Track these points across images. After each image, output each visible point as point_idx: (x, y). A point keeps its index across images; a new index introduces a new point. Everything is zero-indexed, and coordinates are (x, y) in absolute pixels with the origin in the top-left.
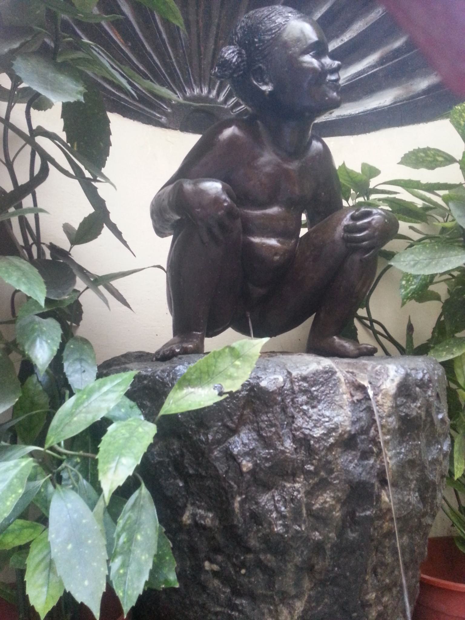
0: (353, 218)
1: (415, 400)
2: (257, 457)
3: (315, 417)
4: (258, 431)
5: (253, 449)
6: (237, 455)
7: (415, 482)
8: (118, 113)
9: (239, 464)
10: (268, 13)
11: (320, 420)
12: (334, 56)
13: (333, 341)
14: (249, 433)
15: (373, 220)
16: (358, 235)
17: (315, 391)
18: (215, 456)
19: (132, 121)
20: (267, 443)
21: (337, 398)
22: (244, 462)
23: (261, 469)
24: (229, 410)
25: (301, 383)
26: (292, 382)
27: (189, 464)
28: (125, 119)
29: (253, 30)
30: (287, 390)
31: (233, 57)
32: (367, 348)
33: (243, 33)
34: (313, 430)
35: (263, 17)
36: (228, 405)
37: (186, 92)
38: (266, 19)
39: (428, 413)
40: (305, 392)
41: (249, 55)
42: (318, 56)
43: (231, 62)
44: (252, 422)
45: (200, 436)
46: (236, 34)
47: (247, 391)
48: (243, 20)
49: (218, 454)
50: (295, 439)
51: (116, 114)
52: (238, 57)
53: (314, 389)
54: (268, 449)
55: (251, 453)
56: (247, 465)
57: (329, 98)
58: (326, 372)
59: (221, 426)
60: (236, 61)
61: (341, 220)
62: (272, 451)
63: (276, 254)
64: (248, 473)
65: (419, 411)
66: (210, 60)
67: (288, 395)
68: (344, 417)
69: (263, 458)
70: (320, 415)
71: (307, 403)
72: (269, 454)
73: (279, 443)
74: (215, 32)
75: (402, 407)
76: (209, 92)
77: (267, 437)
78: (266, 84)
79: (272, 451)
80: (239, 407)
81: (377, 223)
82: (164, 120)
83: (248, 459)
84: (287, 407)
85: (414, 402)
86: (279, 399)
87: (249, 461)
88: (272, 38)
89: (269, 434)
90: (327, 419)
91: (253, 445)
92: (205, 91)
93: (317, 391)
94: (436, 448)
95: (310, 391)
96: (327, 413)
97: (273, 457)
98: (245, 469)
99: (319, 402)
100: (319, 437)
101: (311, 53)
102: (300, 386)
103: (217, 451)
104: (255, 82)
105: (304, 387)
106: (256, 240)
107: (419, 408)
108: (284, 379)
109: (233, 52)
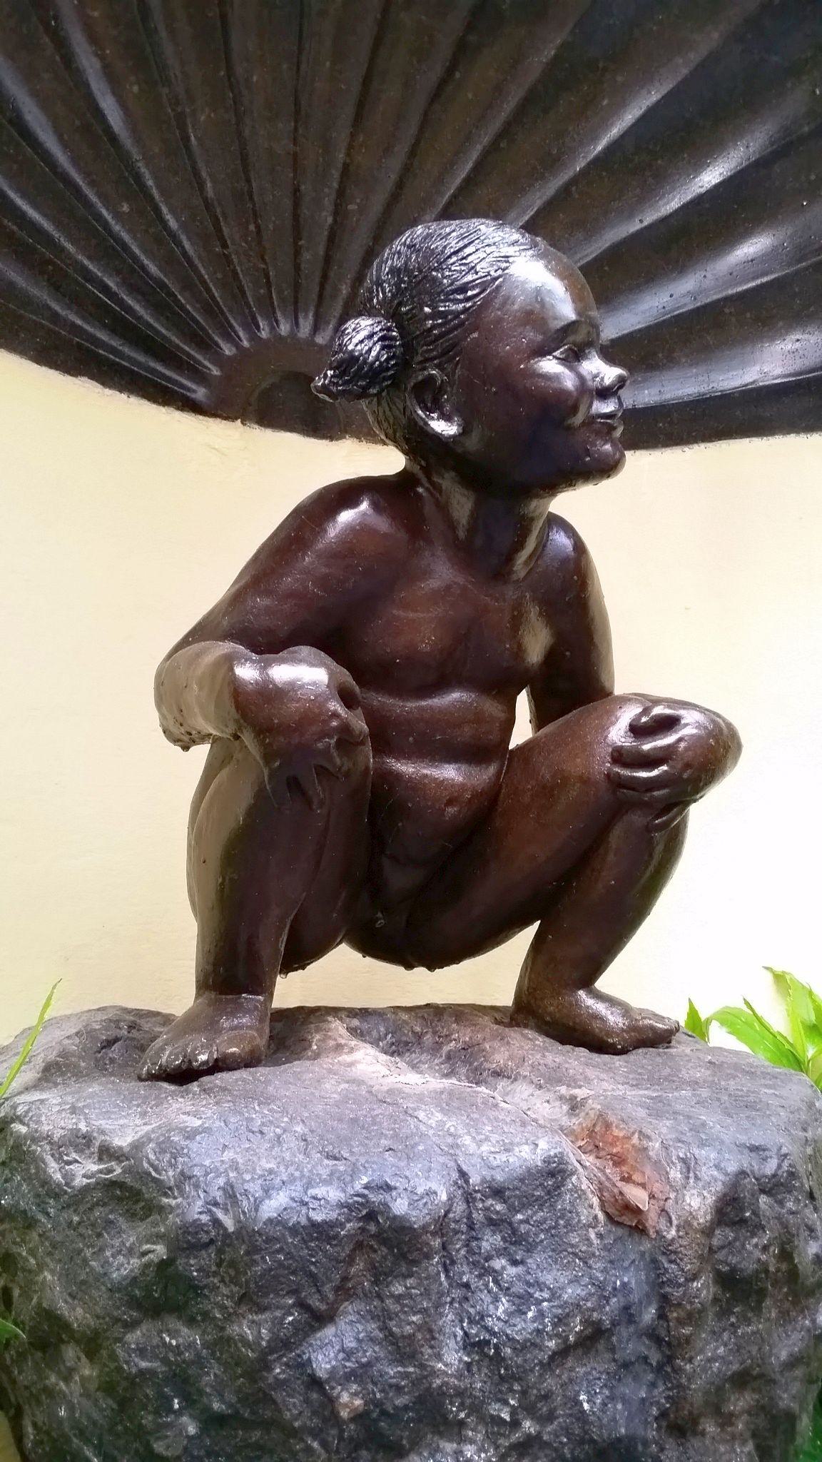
0: (637, 730)
1: (758, 1228)
2: (375, 1384)
3: (519, 1288)
4: (383, 1318)
5: (369, 1365)
6: (328, 1381)
7: (745, 1417)
8: (92, 377)
9: (331, 1401)
10: (461, 244)
11: (531, 1296)
12: (611, 353)
13: (578, 1004)
14: (359, 1322)
15: (680, 740)
16: (643, 774)
17: (521, 1222)
18: (275, 1377)
19: (124, 396)
20: (403, 1349)
21: (574, 1238)
22: (345, 1397)
23: (384, 1413)
24: (312, 1268)
25: (490, 1202)
26: (469, 1198)
27: (212, 1387)
28: (108, 391)
29: (420, 282)
30: (456, 1222)
31: (370, 350)
32: (652, 1028)
33: (397, 285)
34: (512, 1321)
35: (448, 252)
36: (312, 1256)
37: (258, 328)
38: (454, 259)
39: (786, 1255)
40: (494, 1223)
41: (408, 347)
42: (574, 357)
43: (365, 361)
44: (367, 1296)
45: (240, 1326)
46: (379, 283)
47: (360, 1219)
48: (396, 253)
49: (283, 1372)
50: (470, 1345)
51: (85, 379)
52: (383, 348)
53: (519, 1217)
54: (404, 1366)
55: (361, 1374)
56: (349, 1400)
57: (594, 459)
58: (552, 1174)
59: (294, 1305)
60: (377, 358)
61: (604, 729)
62: (411, 1369)
63: (450, 802)
64: (352, 1420)
65: (764, 1257)
66: (321, 252)
67: (456, 1232)
68: (586, 1286)
69: (391, 1386)
70: (529, 1284)
71: (501, 1253)
72: (406, 1375)
73: (430, 1351)
74: (335, 185)
75: (724, 1252)
76: (316, 329)
77: (403, 1337)
78: (447, 418)
79: (411, 1369)
80: (339, 1262)
81: (686, 749)
82: (200, 393)
83: (354, 1387)
84: (453, 1262)
85: (753, 1235)
86: (436, 1243)
87: (356, 1394)
88: (465, 310)
89: (408, 1329)
90: (546, 1295)
91: (370, 1352)
92: (305, 329)
93: (526, 1221)
94: (799, 1327)
95: (510, 1224)
96: (548, 1278)
97: (416, 1383)
98: (344, 1414)
99: (530, 1250)
100: (526, 1340)
101: (557, 353)
102: (487, 1209)
103: (281, 1365)
104: (420, 412)
105: (498, 1213)
106: (406, 768)
107: (765, 1248)
108: (449, 1194)
109: (370, 336)
